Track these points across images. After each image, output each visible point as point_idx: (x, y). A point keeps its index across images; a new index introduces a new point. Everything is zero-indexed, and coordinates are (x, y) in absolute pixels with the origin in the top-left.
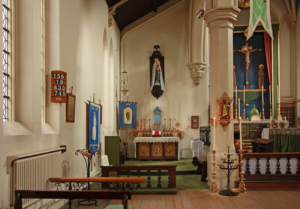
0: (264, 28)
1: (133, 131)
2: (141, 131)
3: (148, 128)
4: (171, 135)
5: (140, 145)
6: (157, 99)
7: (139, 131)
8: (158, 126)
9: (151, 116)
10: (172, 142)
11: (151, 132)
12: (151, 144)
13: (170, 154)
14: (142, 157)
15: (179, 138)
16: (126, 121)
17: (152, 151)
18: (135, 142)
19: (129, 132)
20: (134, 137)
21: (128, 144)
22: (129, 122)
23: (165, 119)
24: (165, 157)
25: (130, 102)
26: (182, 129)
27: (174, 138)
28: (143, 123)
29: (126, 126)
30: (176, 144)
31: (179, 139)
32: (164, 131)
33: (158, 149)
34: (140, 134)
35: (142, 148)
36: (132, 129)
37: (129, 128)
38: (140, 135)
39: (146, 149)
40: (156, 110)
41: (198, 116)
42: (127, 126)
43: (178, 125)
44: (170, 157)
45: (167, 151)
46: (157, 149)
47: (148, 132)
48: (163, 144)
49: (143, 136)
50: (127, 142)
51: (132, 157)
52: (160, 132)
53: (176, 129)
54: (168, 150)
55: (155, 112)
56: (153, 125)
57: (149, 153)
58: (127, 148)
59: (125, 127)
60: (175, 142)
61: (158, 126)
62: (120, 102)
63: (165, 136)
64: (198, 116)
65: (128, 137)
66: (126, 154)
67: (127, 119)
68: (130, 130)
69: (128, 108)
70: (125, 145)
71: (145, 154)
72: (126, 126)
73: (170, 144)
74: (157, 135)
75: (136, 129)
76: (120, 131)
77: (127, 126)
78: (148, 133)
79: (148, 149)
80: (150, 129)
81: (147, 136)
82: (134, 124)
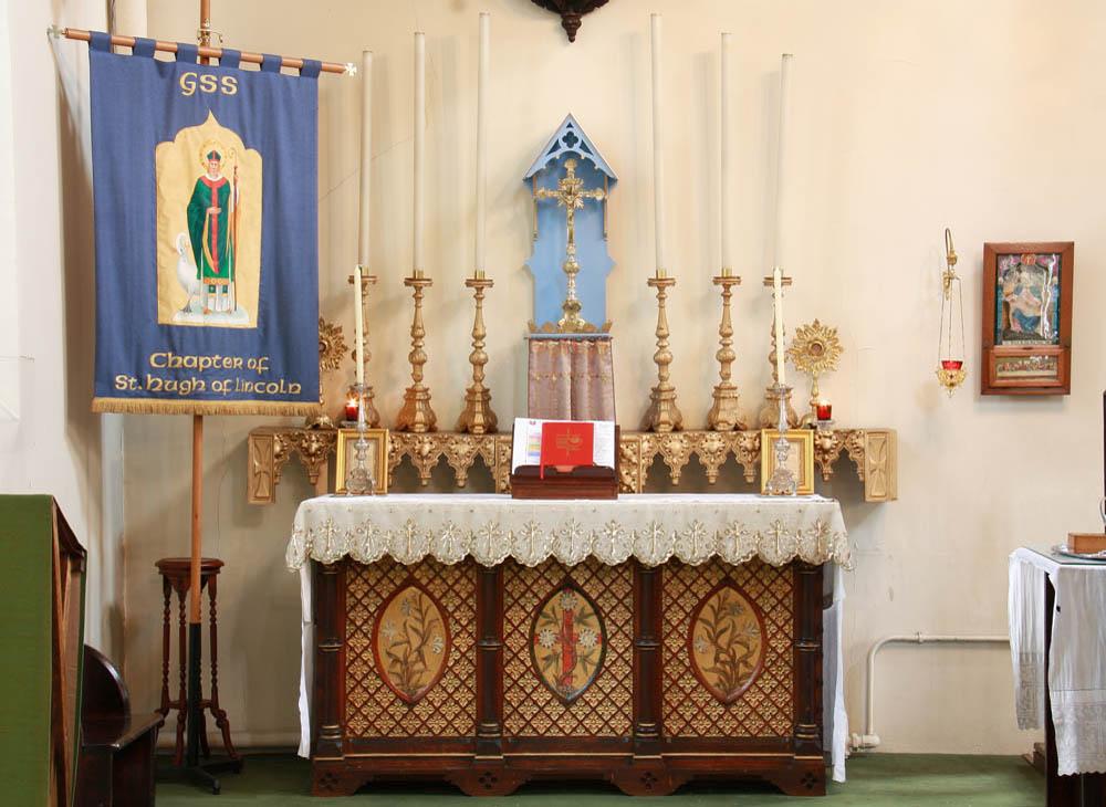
0: (80, 541)
1: (275, 421)
2: (374, 425)
3: (463, 377)
4: (737, 476)
5: (357, 588)
6: (571, 30)
7: (351, 415)
8: (585, 366)
9: (499, 246)
10: (757, 565)
11: (491, 429)
12: (491, 587)
13: (727, 704)
14: (384, 743)
15: (837, 504)
16: (185, 294)
17: (513, 669)
18: (296, 561)
19: (223, 435)
20: (285, 490)
21: (222, 578)
22: (219, 303)
23: (660, 283)
24: (659, 743)
25: (230, 60)
26: (859, 399)
27: (777, 518)
28: (405, 319)
29: (182, 361)
30: (807, 586)
31: (838, 517)
32: (649, 427)
33: (588, 639)
34: (358, 454)
35: (390, 631)
36: (266, 397)
37: (221, 386)
38: (368, 464)
39: (438, 643)
40: (552, 162)
41: (1071, 246)
42: (199, 362)
43: (817, 349)
44: (727, 743)
45: (697, 675)
46: (568, 639)
47: (465, 430)
48: (647, 585)
49: (405, 477)
50: (208, 551)
51: (271, 739)
52: (603, 435)
53: (799, 403)
54: (705, 661)
55: (542, 191)
56: (516, 350)
57: (464, 697)
58: (196, 628)
59: (177, 374)
60: (796, 564)
61: (575, 356)
62: (100, 44)
63: (659, 478)
64: (1071, 246)
65: (218, 498)
66: (193, 707)
67: (204, 272)
68: (245, 414)
69: (213, 134)
70: (174, 596)
71: (422, 709)
72: (182, 361)
73: (728, 582)
74: (568, 474)
75: (311, 394)
76: (111, 425)
77: (199, 362)
78: (464, 448)
79: (463, 642)
80: (479, 397)
81: (445, 480)
82: (292, 338)
